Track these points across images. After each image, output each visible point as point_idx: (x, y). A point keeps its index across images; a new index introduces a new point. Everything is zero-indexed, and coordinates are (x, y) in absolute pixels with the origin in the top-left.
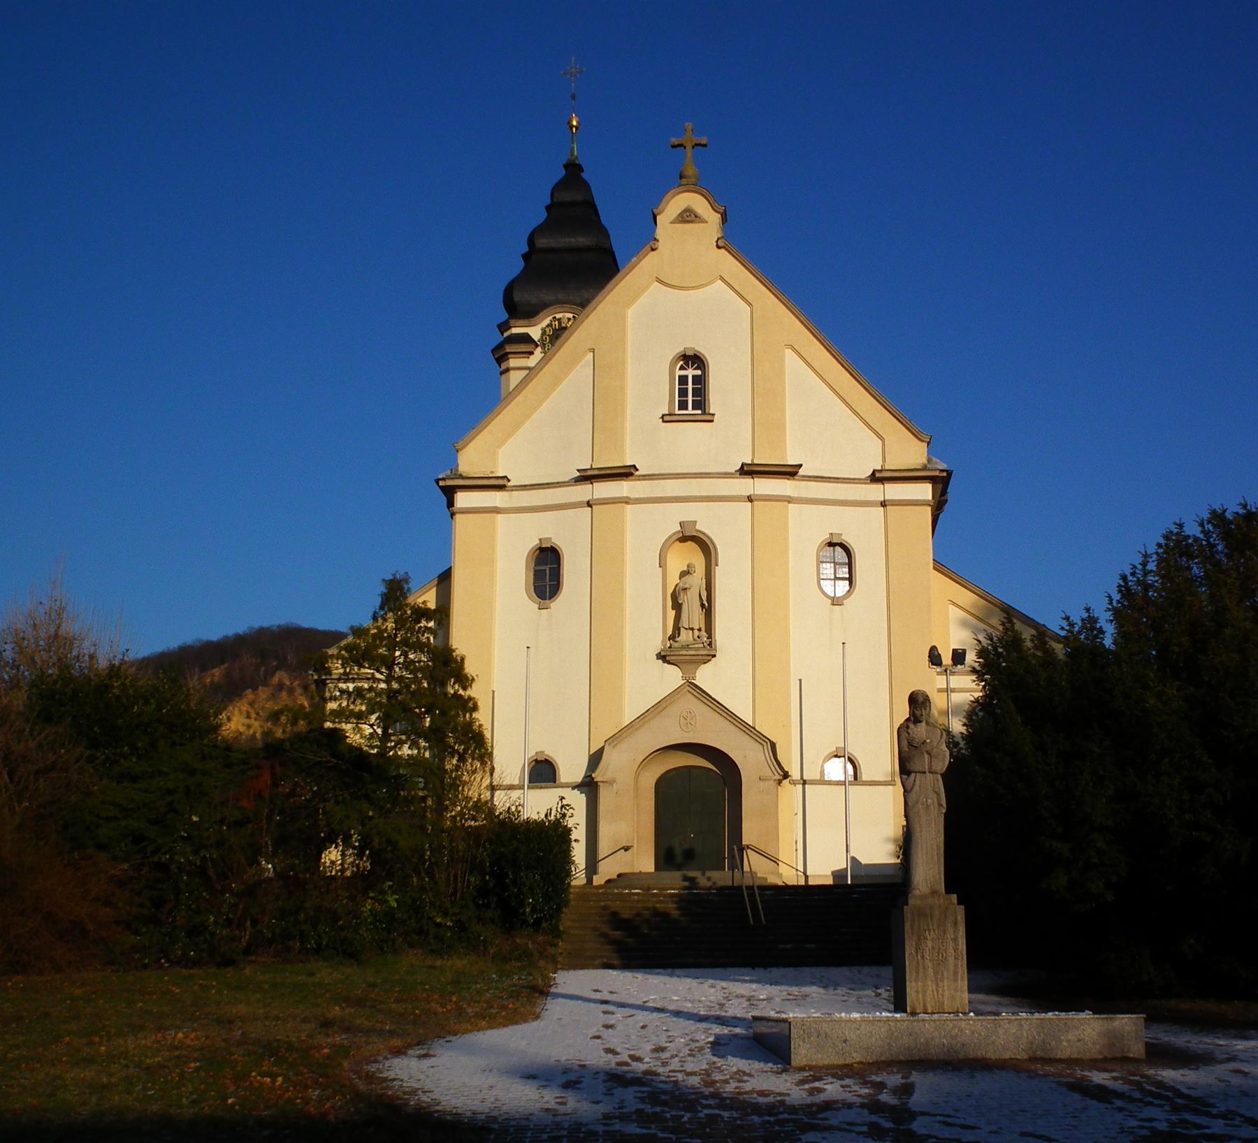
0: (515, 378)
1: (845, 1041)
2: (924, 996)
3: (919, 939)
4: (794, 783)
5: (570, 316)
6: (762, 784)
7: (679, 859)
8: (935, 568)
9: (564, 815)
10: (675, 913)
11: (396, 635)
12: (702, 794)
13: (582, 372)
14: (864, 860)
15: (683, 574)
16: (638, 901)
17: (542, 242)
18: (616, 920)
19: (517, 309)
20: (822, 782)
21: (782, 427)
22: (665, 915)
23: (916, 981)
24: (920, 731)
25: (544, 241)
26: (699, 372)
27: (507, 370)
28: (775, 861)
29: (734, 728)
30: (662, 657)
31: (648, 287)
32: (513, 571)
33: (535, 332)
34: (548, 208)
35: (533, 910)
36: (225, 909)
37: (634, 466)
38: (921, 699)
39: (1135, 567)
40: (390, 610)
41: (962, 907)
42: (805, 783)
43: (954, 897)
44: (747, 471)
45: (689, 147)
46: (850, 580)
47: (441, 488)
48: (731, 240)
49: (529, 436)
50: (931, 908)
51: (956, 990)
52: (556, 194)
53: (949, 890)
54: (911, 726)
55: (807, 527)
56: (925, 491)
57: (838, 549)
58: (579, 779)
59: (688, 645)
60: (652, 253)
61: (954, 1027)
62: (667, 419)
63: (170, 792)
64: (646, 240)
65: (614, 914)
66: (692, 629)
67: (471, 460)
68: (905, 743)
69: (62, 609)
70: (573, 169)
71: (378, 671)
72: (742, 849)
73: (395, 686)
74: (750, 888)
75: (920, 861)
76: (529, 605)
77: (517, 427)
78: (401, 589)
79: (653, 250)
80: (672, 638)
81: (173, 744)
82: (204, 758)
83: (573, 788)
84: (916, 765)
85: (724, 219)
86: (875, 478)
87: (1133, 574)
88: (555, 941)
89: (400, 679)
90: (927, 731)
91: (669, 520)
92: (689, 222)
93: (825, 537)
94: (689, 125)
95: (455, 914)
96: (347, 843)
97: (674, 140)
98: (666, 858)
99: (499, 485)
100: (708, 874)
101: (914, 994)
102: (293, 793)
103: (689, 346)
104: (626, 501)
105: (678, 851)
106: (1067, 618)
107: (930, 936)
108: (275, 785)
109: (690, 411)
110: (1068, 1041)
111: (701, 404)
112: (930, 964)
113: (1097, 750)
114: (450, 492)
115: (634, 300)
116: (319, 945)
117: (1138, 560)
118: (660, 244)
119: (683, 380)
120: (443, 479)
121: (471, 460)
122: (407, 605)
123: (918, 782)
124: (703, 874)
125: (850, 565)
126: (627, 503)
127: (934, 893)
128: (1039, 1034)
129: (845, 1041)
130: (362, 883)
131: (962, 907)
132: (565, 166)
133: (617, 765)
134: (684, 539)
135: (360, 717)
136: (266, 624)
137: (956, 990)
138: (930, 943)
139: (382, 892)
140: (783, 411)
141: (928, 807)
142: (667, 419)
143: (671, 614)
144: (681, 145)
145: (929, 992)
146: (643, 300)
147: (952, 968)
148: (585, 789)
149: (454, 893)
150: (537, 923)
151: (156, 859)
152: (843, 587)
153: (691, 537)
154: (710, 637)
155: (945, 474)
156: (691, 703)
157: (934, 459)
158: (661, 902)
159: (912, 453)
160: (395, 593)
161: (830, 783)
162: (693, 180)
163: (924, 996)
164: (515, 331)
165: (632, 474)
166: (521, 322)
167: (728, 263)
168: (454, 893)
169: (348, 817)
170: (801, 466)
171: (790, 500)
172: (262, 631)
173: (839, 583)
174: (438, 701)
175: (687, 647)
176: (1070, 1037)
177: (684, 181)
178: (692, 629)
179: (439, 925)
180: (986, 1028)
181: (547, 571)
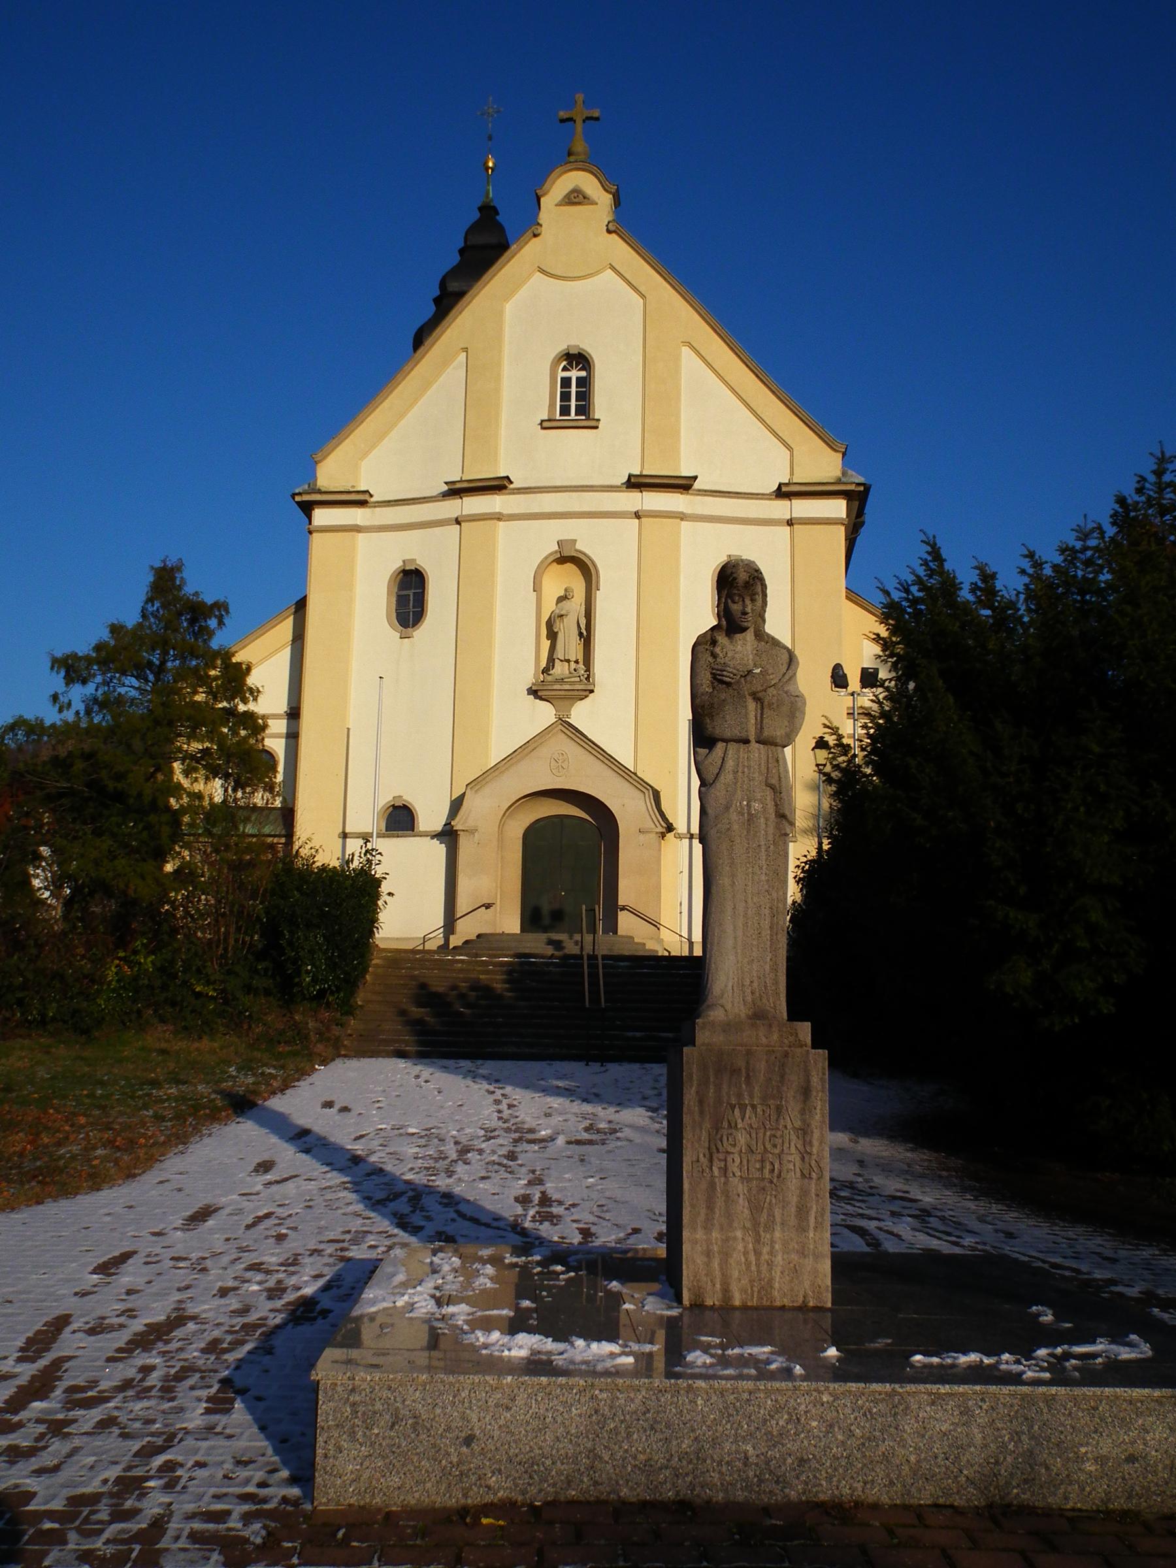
1: (469, 1440)
2: (724, 1262)
3: (717, 1128)
4: (680, 837)
6: (642, 837)
7: (546, 921)
8: (847, 598)
10: (499, 986)
13: (454, 374)
15: (560, 600)
16: (461, 970)
18: (426, 996)
21: (676, 434)
22: (485, 991)
23: (707, 1228)
26: (583, 374)
28: (656, 925)
29: (610, 772)
30: (533, 692)
31: (525, 281)
32: (373, 596)
34: (461, 252)
35: (315, 981)
37: (508, 477)
38: (742, 576)
39: (1143, 479)
41: (823, 1053)
43: (805, 1030)
44: (635, 483)
45: (579, 125)
49: (393, 449)
51: (802, 1253)
53: (795, 1014)
54: (722, 639)
56: (838, 508)
58: (439, 827)
61: (778, 1409)
62: (545, 425)
64: (530, 224)
65: (423, 986)
66: (568, 661)
67: (331, 473)
68: (705, 678)
74: (593, 957)
75: (730, 943)
76: (389, 633)
77: (382, 435)
79: (535, 236)
80: (545, 671)
83: (433, 837)
84: (727, 725)
86: (782, 493)
87: (1140, 491)
90: (758, 653)
91: (545, 539)
92: (579, 203)
94: (580, 97)
97: (563, 114)
98: (532, 919)
99: (360, 500)
101: (700, 1260)
103: (573, 343)
104: (499, 517)
105: (546, 909)
106: (1031, 555)
110: (1101, 1460)
112: (741, 1188)
113: (1096, 749)
114: (307, 508)
115: (513, 292)
116: (43, 1016)
117: (1147, 468)
118: (544, 230)
119: (566, 382)
120: (300, 494)
121: (331, 473)
123: (730, 764)
126: (499, 519)
127: (759, 1016)
128: (1016, 1435)
129: (469, 1440)
131: (823, 1053)
132: (480, 209)
133: (483, 811)
134: (562, 560)
137: (802, 1253)
138: (742, 1139)
141: (751, 818)
142: (545, 425)
144: (571, 119)
145: (737, 1257)
146: (523, 292)
147: (794, 1200)
148: (446, 838)
153: (570, 558)
155: (862, 488)
156: (563, 744)
158: (488, 972)
159: (824, 464)
162: (582, 157)
163: (724, 1262)
165: (505, 487)
167: (620, 250)
170: (695, 478)
171: (682, 517)
175: (561, 681)
177: (572, 159)
178: (568, 661)
179: (199, 995)
180: (868, 1414)
181: (410, 595)
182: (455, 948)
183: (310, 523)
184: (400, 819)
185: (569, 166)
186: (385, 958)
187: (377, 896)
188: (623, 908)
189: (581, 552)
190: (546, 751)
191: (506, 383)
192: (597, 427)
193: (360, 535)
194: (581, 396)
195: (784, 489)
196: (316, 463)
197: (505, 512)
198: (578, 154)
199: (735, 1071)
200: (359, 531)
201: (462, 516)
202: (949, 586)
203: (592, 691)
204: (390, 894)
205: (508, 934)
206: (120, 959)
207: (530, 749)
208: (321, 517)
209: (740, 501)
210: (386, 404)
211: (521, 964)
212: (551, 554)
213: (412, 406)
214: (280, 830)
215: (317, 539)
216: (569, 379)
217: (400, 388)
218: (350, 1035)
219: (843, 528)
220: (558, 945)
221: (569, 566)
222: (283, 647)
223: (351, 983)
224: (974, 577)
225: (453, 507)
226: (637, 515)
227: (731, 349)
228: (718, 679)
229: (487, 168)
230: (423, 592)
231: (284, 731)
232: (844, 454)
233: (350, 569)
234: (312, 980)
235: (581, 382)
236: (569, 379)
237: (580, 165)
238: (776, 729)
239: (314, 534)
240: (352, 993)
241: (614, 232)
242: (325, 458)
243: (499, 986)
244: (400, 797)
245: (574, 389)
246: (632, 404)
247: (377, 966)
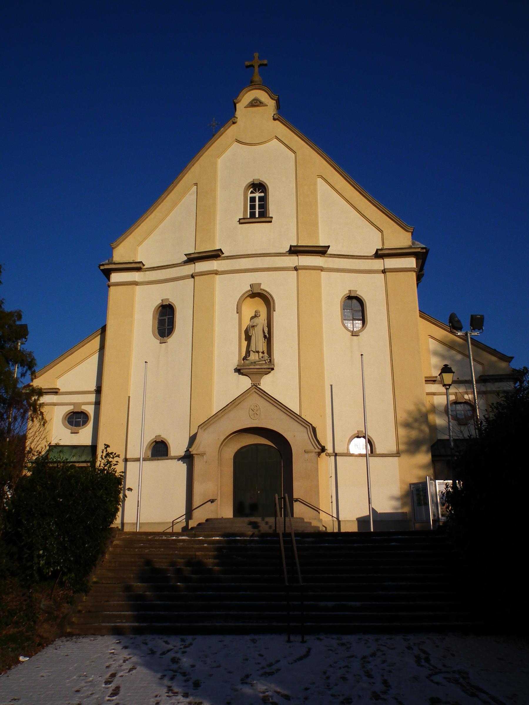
4: (329, 455)
6: (306, 456)
12: (265, 463)
13: (190, 198)
14: (380, 510)
15: (252, 318)
18: (151, 573)
22: (196, 565)
26: (262, 194)
28: (317, 510)
30: (238, 371)
31: (229, 146)
32: (144, 320)
35: (48, 564)
37: (220, 250)
42: (336, 455)
44: (294, 251)
45: (256, 69)
49: (155, 241)
55: (334, 288)
56: (411, 262)
57: (355, 301)
58: (182, 454)
59: (256, 362)
60: (233, 125)
62: (241, 222)
65: (148, 563)
66: (258, 352)
72: (292, 500)
77: (150, 233)
79: (234, 123)
80: (245, 359)
86: (379, 255)
91: (243, 284)
93: (346, 292)
94: (256, 55)
97: (247, 63)
98: (239, 509)
99: (138, 267)
100: (267, 519)
104: (216, 273)
114: (107, 273)
115: (223, 152)
119: (253, 199)
120: (103, 265)
121: (121, 253)
124: (263, 520)
126: (216, 274)
133: (208, 442)
140: (317, 215)
142: (241, 222)
143: (245, 344)
144: (252, 66)
146: (228, 153)
153: (258, 294)
155: (424, 251)
156: (255, 400)
159: (402, 239)
161: (352, 455)
165: (219, 256)
170: (329, 247)
171: (322, 269)
177: (253, 84)
178: (258, 352)
181: (165, 319)
182: (192, 528)
183: (109, 281)
184: (159, 449)
185: (251, 88)
188: (297, 500)
189: (264, 290)
192: (271, 222)
193: (137, 287)
194: (260, 207)
195: (379, 252)
196: (113, 248)
197: (219, 270)
200: (137, 285)
201: (195, 273)
203: (273, 369)
205: (225, 519)
207: (237, 403)
208: (115, 277)
209: (354, 260)
210: (152, 216)
211: (229, 542)
212: (246, 292)
214: (89, 458)
215: (112, 289)
216: (255, 198)
217: (160, 207)
218: (80, 611)
219: (414, 274)
220: (255, 525)
221: (258, 300)
222: (94, 353)
223: (85, 563)
225: (190, 269)
230: (173, 317)
231: (94, 400)
232: (412, 235)
233: (132, 306)
234: (46, 563)
236: (255, 198)
237: (257, 87)
243: (211, 560)
244: (160, 436)
246: (290, 208)
247: (117, 546)
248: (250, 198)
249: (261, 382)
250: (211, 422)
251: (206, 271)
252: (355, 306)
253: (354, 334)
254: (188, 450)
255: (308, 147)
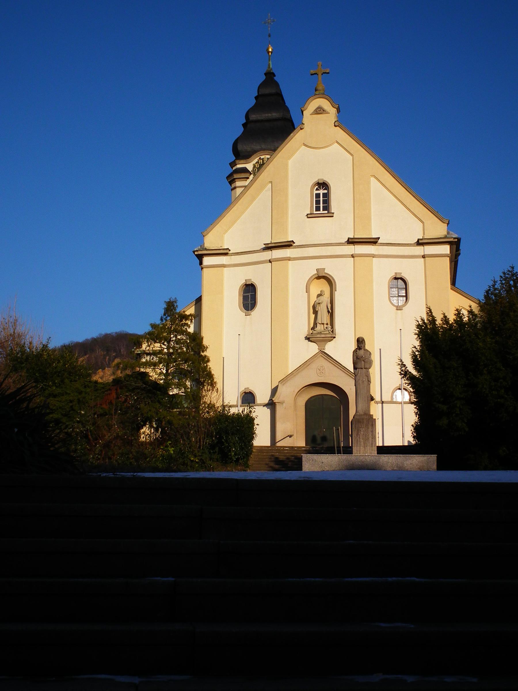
0: (239, 191)
3: (358, 431)
4: (377, 403)
5: (269, 156)
9: (251, 412)
11: (171, 327)
13: (266, 194)
15: (319, 296)
17: (253, 117)
19: (240, 154)
20: (392, 402)
21: (369, 219)
24: (361, 353)
25: (254, 116)
26: (326, 191)
27: (235, 188)
30: (308, 339)
32: (233, 297)
33: (250, 167)
35: (235, 454)
36: (97, 452)
37: (293, 241)
39: (490, 287)
40: (168, 316)
42: (383, 403)
44: (351, 242)
45: (320, 76)
46: (406, 296)
47: (196, 255)
48: (341, 122)
50: (363, 419)
52: (260, 90)
54: (358, 351)
55: (383, 270)
56: (446, 249)
57: (400, 281)
58: (266, 401)
59: (321, 332)
62: (308, 216)
63: (71, 401)
65: (277, 458)
66: (323, 324)
67: (211, 241)
68: (355, 357)
69: (16, 320)
70: (270, 75)
71: (163, 344)
73: (171, 351)
76: (240, 313)
77: (234, 222)
78: (173, 306)
79: (301, 129)
80: (313, 329)
81: (71, 381)
82: (85, 387)
83: (264, 406)
84: (359, 366)
85: (339, 111)
86: (419, 243)
88: (246, 469)
89: (173, 348)
90: (364, 353)
91: (311, 268)
93: (393, 275)
94: (320, 63)
95: (200, 456)
96: (151, 426)
97: (312, 72)
101: (356, 452)
102: (126, 400)
104: (289, 259)
107: (362, 430)
108: (118, 398)
109: (321, 212)
111: (327, 208)
112: (362, 441)
113: (455, 365)
114: (200, 257)
115: (292, 155)
117: (491, 283)
118: (305, 126)
119: (318, 196)
120: (197, 251)
121: (211, 241)
122: (176, 313)
125: (406, 289)
126: (289, 260)
130: (157, 443)
132: (265, 74)
133: (286, 394)
134: (319, 278)
135: (155, 365)
136: (109, 332)
138: (362, 432)
139: (167, 446)
141: (363, 381)
142: (308, 216)
143: (313, 316)
144: (316, 74)
146: (297, 155)
149: (200, 447)
150: (237, 460)
151: (66, 431)
152: (402, 300)
153: (322, 277)
154: (332, 328)
155: (456, 240)
156: (322, 362)
157: (451, 232)
159: (438, 229)
160: (170, 307)
162: (322, 92)
164: (239, 166)
165: (291, 245)
166: (242, 161)
167: (340, 134)
168: (200, 447)
169: (150, 410)
170: (379, 238)
171: (373, 256)
172: (107, 336)
173: (401, 298)
174: (193, 362)
175: (320, 333)
176: (408, 462)
177: (317, 93)
178: (323, 324)
179: (192, 461)
181: (249, 296)
185: (316, 96)
186: (257, 449)
187: (253, 424)
189: (327, 274)
190: (314, 366)
191: (290, 197)
194: (325, 202)
198: (320, 90)
199: (360, 422)
200: (225, 267)
202: (433, 321)
203: (335, 337)
204: (257, 425)
206: (162, 449)
207: (307, 364)
212: (314, 275)
213: (247, 208)
216: (320, 194)
219: (448, 258)
221: (323, 281)
224: (442, 316)
226: (353, 256)
227: (394, 178)
228: (357, 358)
229: (269, 52)
232: (448, 224)
235: (325, 195)
236: (320, 194)
238: (367, 366)
239: (204, 269)
240: (248, 460)
241: (338, 126)
242: (208, 234)
245: (321, 199)
246: (349, 205)
248: (316, 194)
249: (326, 347)
250: (288, 379)
251: (280, 258)
252: (400, 281)
253: (399, 308)
254: (271, 400)
255: (364, 150)
